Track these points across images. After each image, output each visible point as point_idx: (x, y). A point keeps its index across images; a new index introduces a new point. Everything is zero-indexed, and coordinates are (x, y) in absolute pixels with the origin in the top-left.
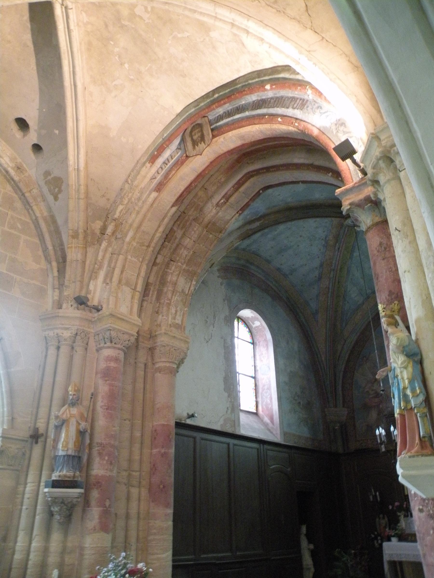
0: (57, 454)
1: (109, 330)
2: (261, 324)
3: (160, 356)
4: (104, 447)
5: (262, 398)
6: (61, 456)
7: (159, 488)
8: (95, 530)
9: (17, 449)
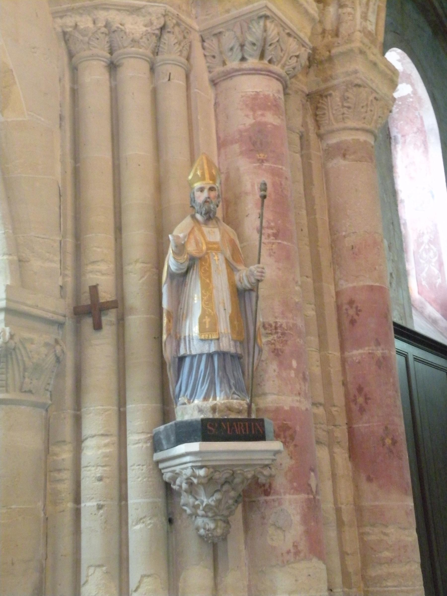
0: (182, 352)
1: (261, 17)
2: (415, 92)
3: (343, 114)
4: (283, 334)
5: (417, 263)
6: (201, 355)
7: (384, 445)
8: (297, 553)
9: (47, 344)
